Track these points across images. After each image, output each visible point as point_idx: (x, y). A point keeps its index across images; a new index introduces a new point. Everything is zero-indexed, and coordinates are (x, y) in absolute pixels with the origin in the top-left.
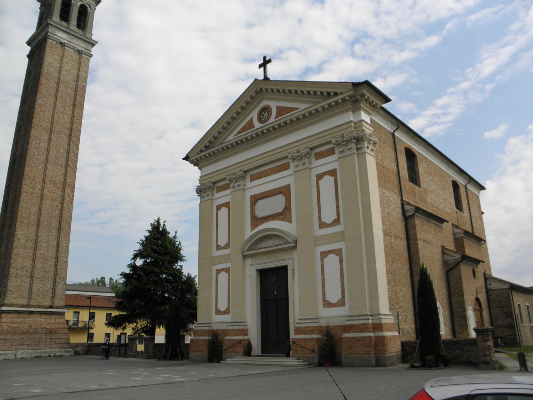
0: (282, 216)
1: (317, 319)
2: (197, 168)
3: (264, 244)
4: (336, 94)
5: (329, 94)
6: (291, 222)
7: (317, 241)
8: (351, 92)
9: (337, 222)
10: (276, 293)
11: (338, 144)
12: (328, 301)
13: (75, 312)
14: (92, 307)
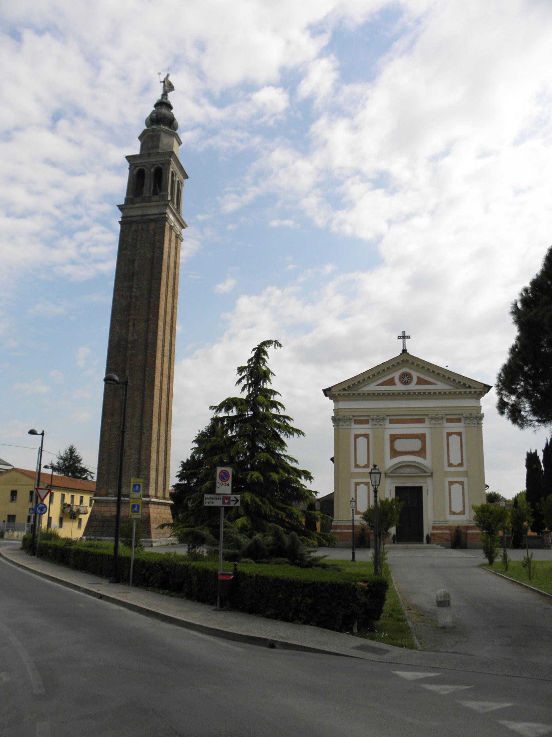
0: (419, 454)
1: (446, 521)
2: (332, 401)
3: (402, 470)
4: (470, 387)
5: (464, 384)
6: (426, 459)
7: (446, 474)
8: (481, 390)
9: (461, 465)
10: (243, 487)
11: (466, 418)
12: (453, 511)
13: (62, 494)
14: (53, 486)
